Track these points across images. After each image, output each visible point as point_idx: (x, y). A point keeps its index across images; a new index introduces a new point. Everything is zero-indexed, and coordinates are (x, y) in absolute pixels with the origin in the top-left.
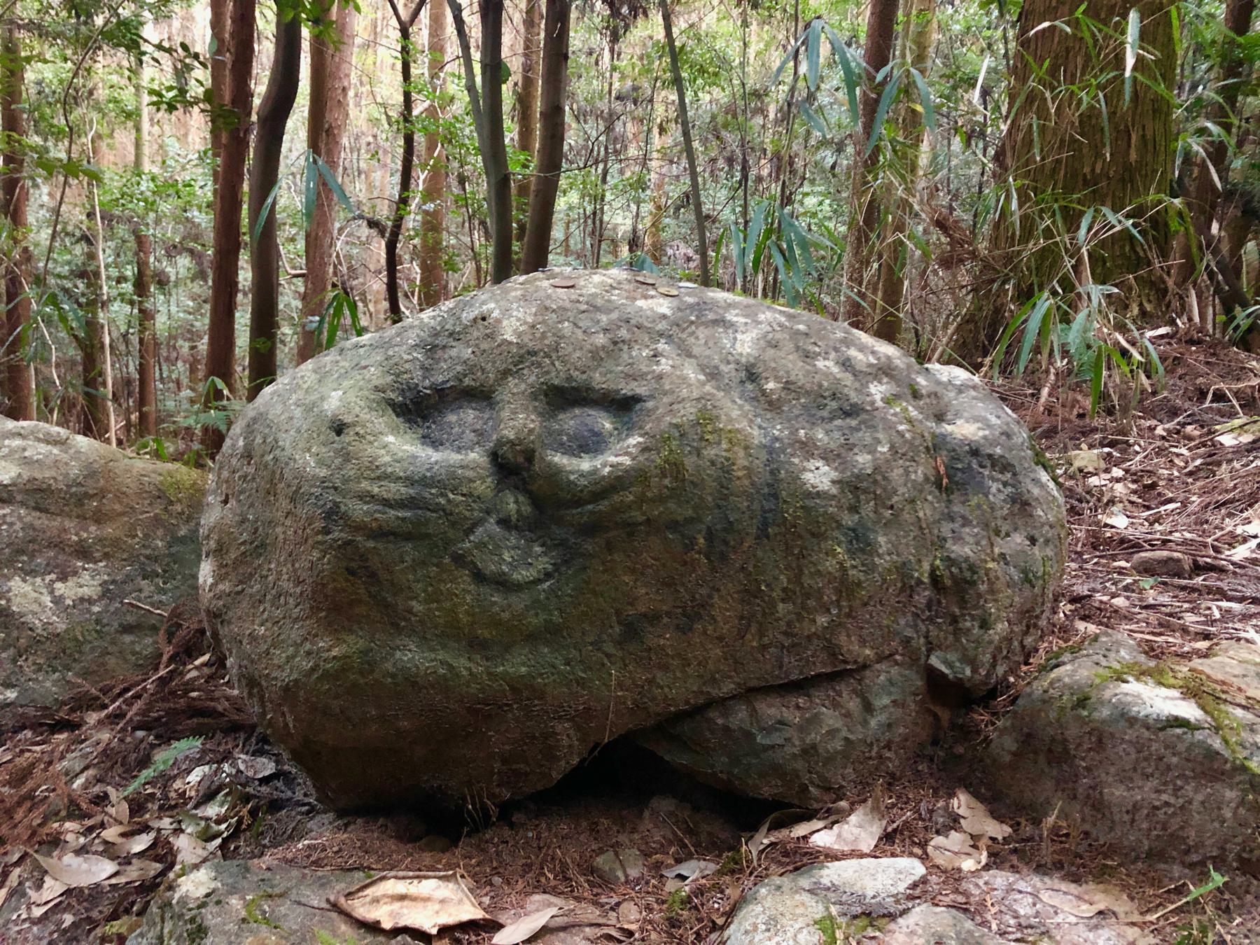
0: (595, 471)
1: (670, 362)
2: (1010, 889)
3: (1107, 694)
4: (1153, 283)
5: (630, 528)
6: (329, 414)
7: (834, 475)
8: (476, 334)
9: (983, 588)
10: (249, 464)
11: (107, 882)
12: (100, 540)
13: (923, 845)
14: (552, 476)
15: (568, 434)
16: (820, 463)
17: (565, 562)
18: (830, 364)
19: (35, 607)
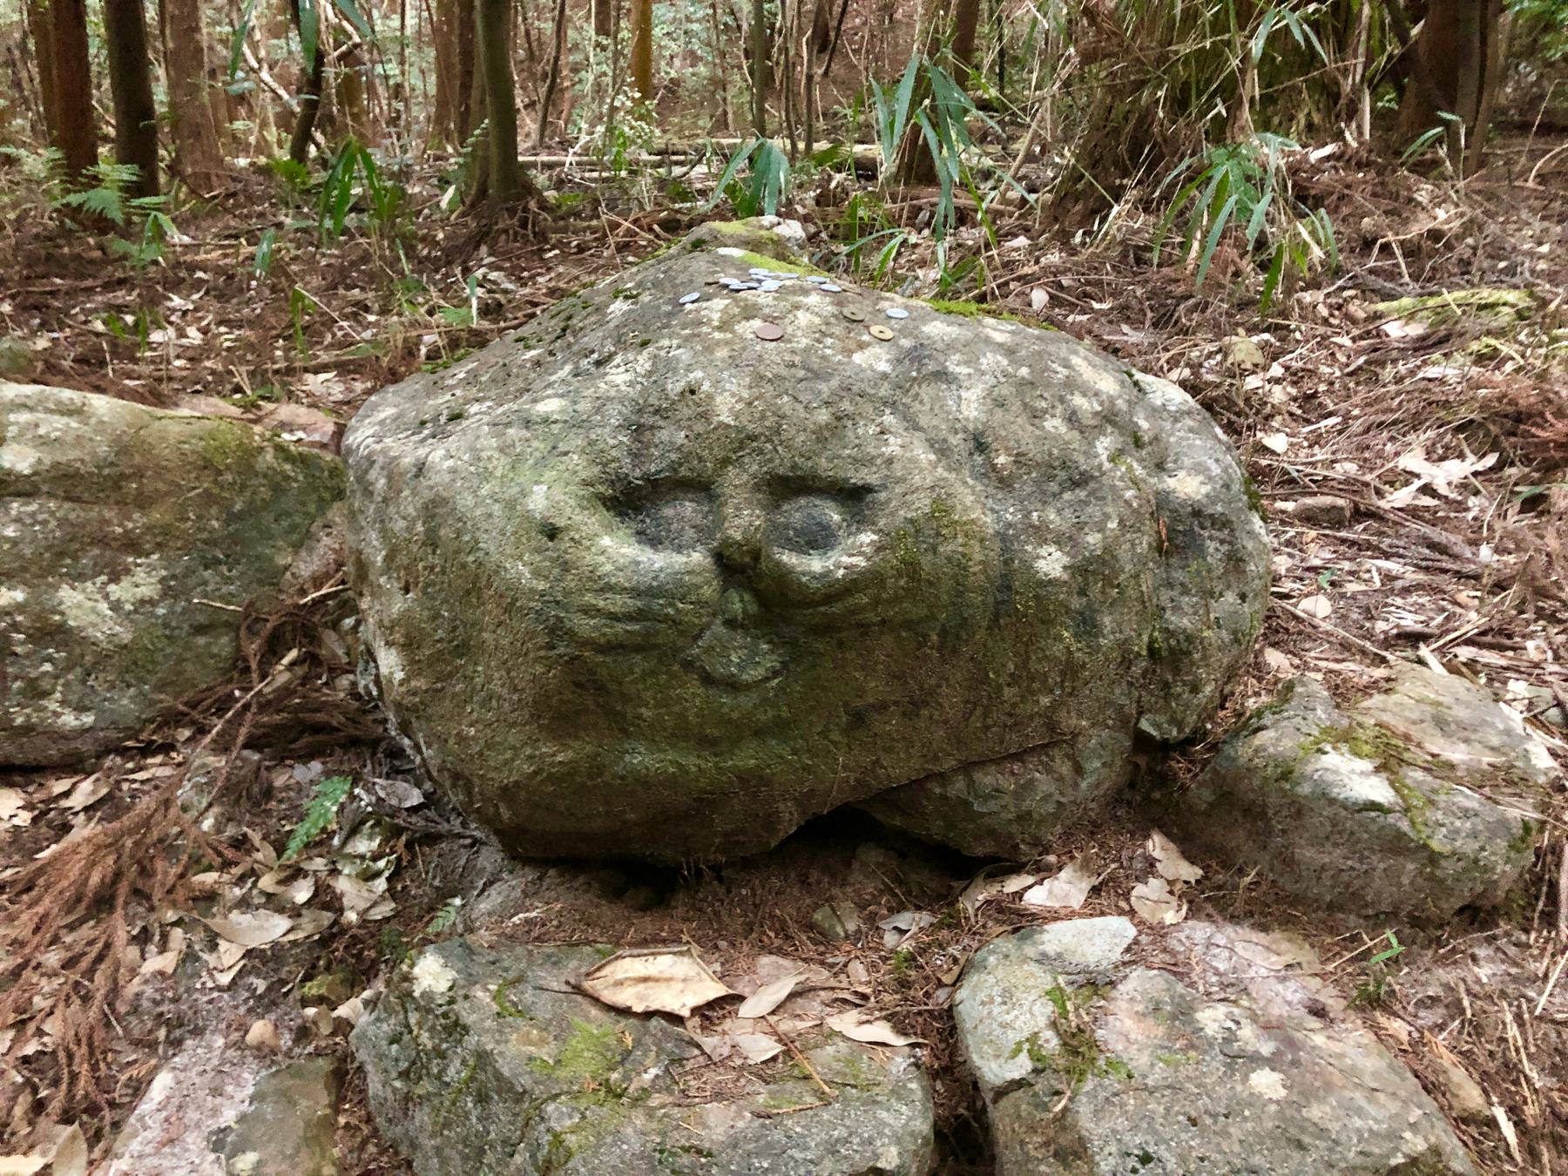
0: (827, 573)
1: (899, 441)
2: (1209, 944)
3: (1309, 769)
4: (1324, 87)
5: (864, 629)
6: (538, 516)
7: (1066, 560)
8: (687, 412)
9: (1196, 656)
10: (434, 552)
11: (285, 939)
12: (149, 529)
13: (1126, 896)
14: (781, 576)
15: (795, 529)
16: (1052, 549)
17: (793, 660)
18: (1057, 422)
19: (93, 618)
